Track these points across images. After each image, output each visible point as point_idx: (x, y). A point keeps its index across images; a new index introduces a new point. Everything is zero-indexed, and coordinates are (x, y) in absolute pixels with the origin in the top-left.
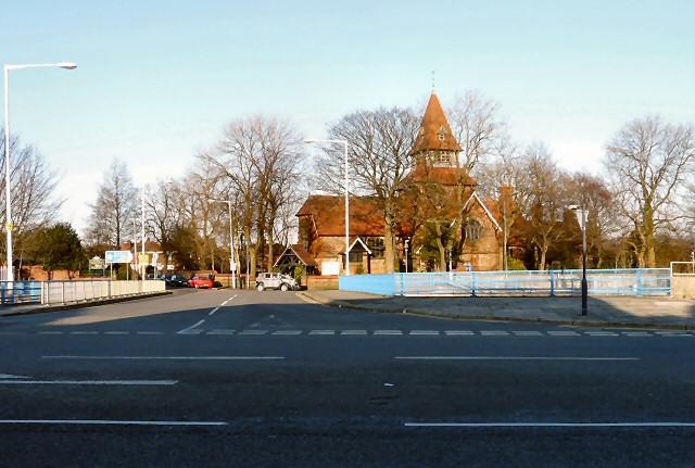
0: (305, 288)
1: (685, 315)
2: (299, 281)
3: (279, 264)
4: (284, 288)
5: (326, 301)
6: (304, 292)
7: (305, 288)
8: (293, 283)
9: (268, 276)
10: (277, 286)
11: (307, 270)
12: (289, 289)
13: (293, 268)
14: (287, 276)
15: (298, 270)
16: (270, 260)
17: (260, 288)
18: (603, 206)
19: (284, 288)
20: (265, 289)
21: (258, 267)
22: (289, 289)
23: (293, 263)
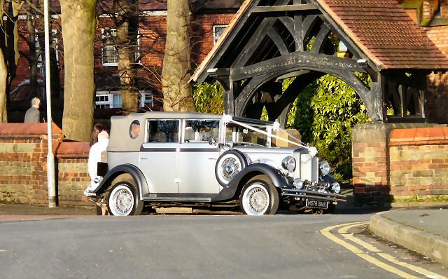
0: (375, 200)
1: (390, 194)
2: (340, 159)
3: (227, 59)
4: (256, 200)
5: (388, 255)
6: (376, 221)
7: (375, 200)
8: (306, 170)
9: (163, 132)
10: (211, 186)
11: (389, 98)
12: (287, 204)
13: (307, 81)
14: (275, 131)
15: (334, 93)
16: (176, 41)
17: (120, 201)
18: (34, 188)
19: (256, 200)
20: (147, 208)
21: (104, 78)
22: (287, 204)
23: (305, 57)
